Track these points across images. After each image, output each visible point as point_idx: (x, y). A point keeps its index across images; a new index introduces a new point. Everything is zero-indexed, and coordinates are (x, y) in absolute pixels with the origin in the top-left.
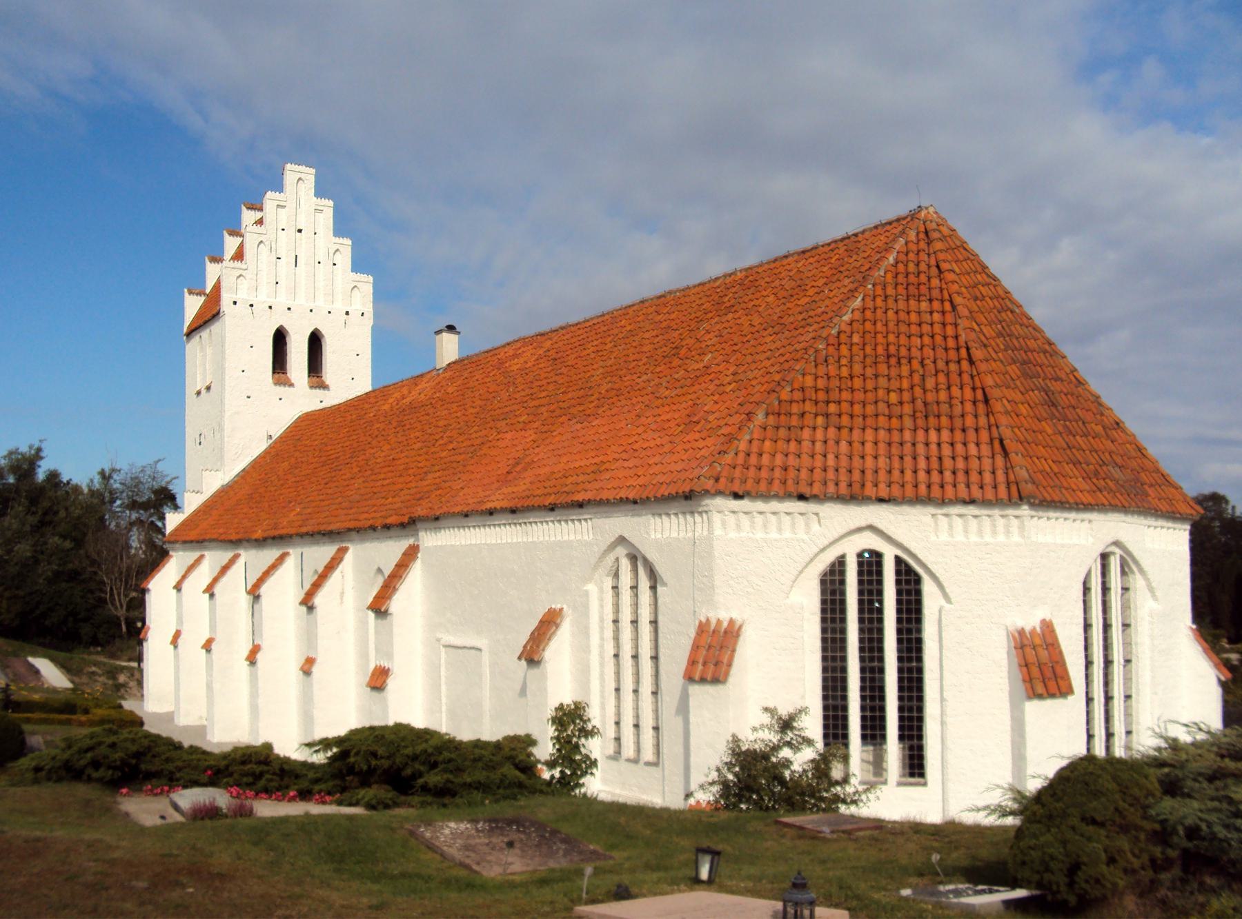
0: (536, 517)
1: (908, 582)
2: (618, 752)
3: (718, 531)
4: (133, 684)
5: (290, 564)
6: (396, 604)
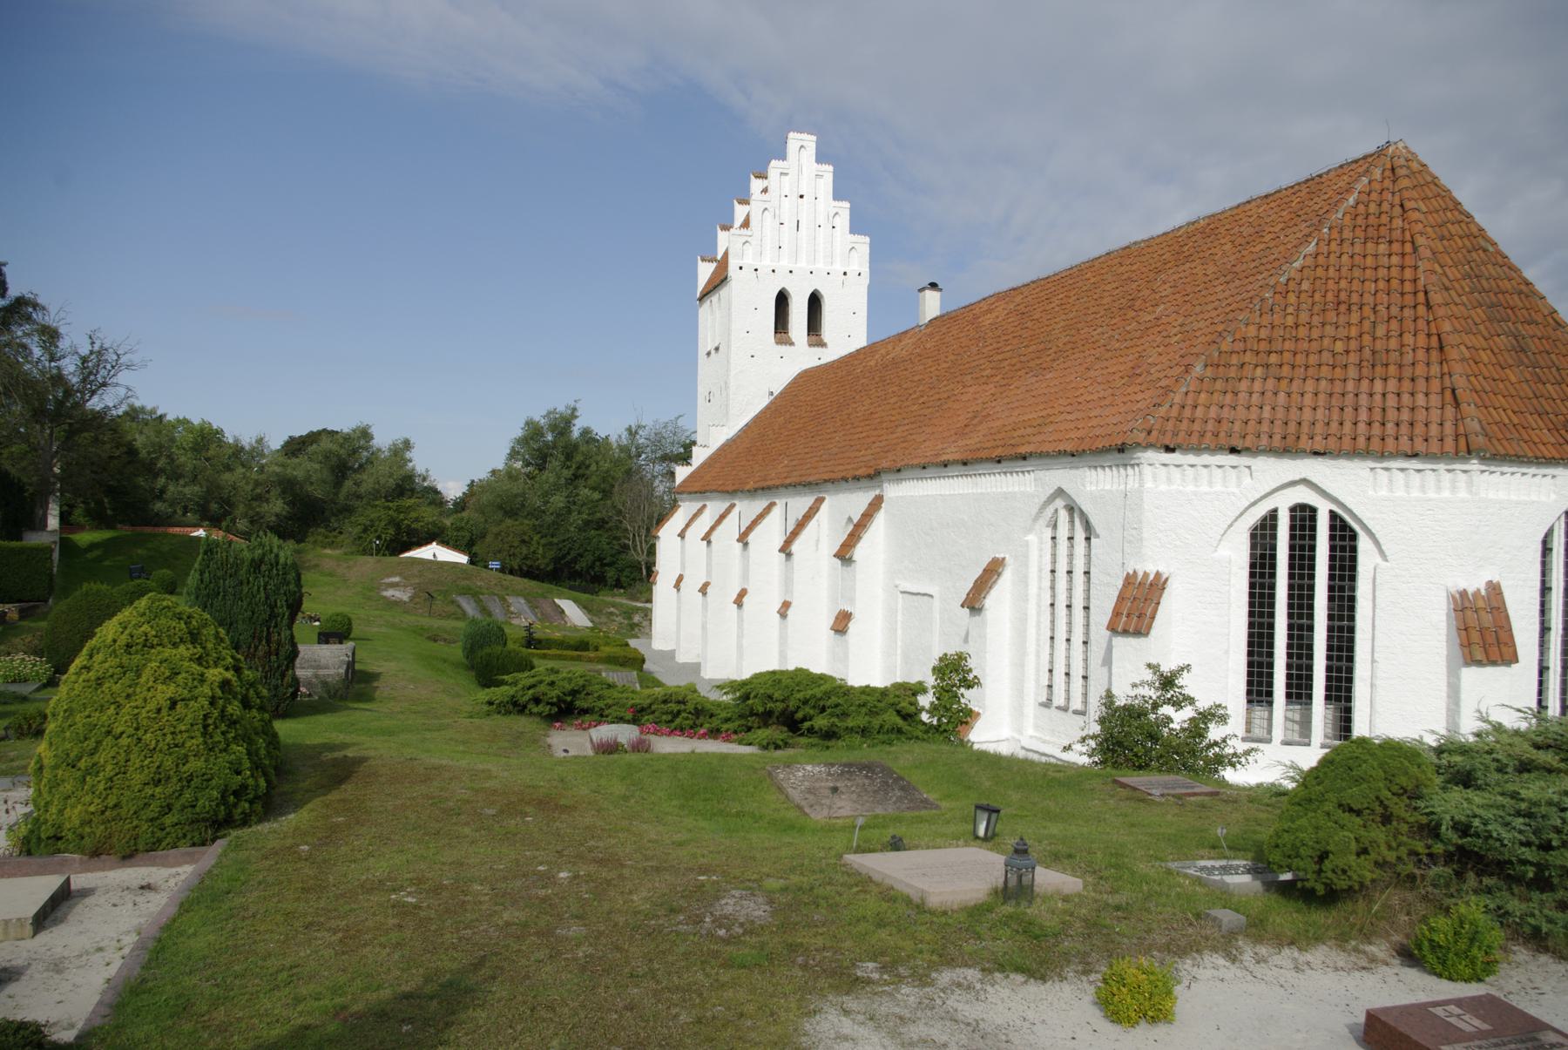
0: (986, 469)
1: (1343, 538)
2: (1049, 700)
3: (1149, 484)
4: (645, 623)
5: (777, 512)
6: (859, 552)
